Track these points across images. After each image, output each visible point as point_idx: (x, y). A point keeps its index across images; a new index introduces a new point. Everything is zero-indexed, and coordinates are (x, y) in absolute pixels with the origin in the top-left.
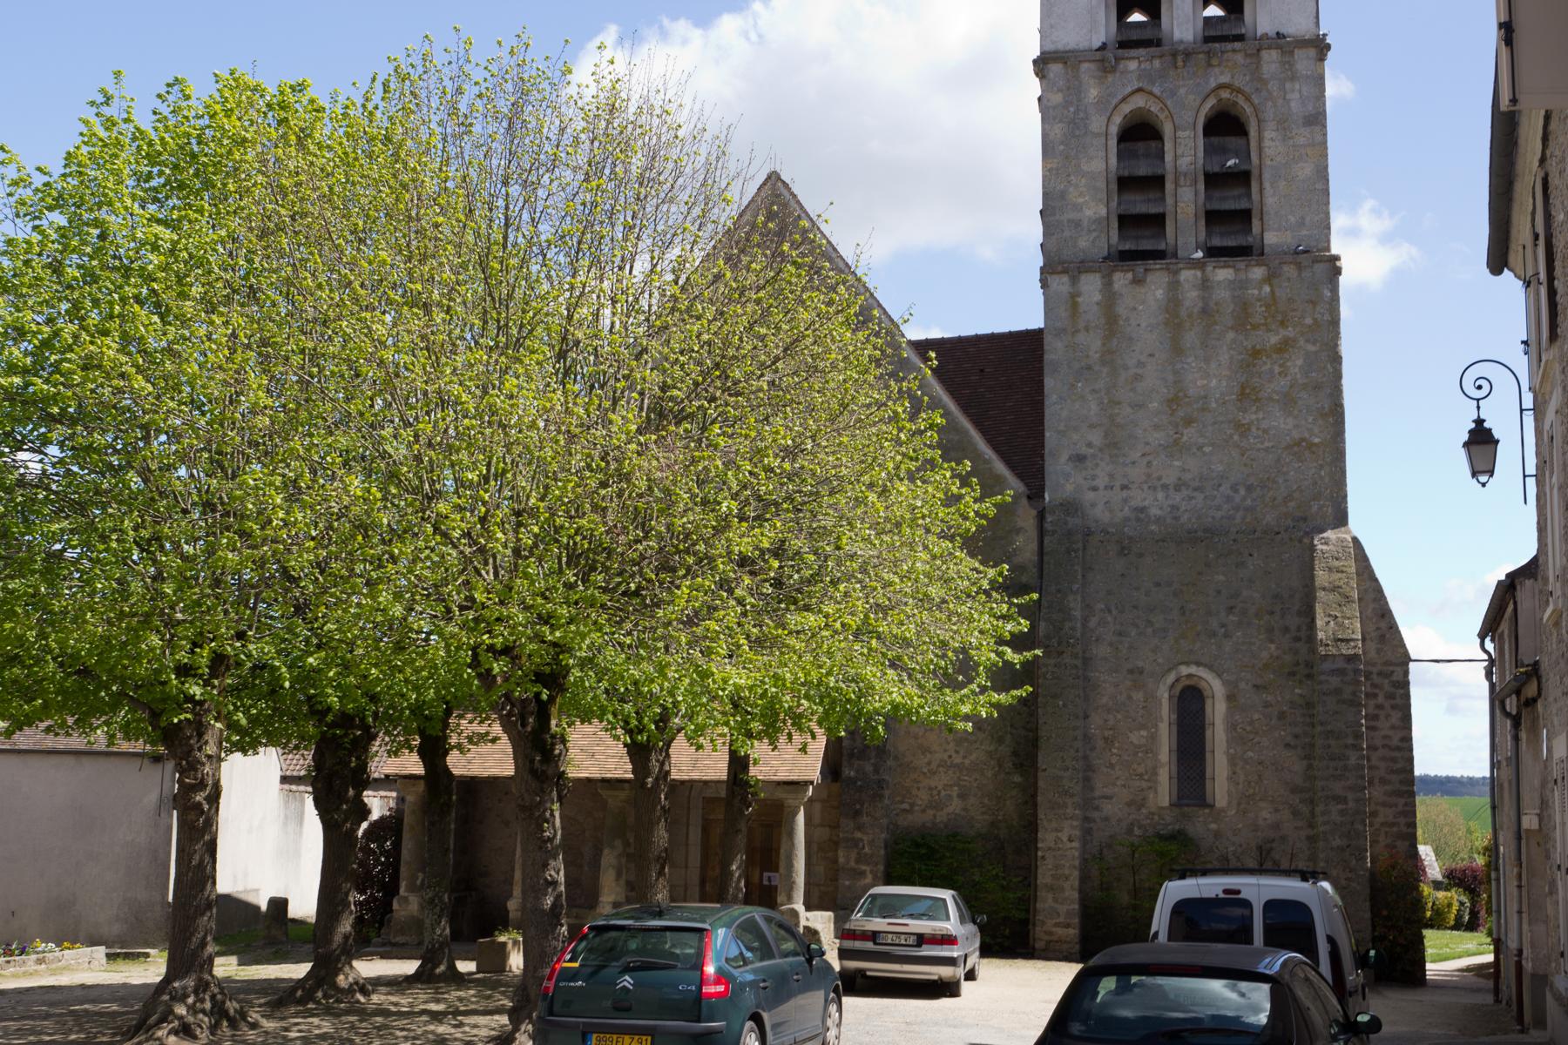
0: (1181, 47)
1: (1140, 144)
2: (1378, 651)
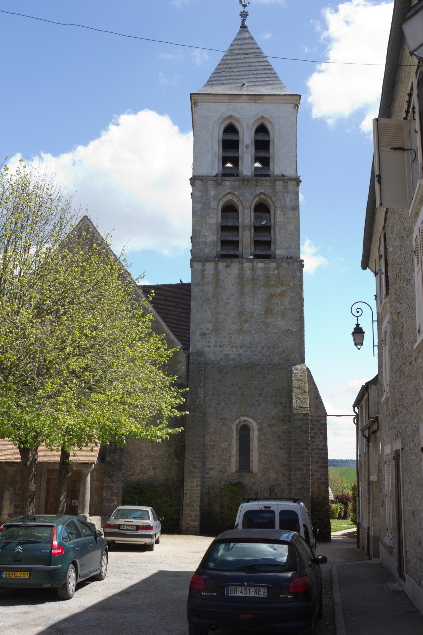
0: (246, 178)
1: (230, 213)
2: (316, 412)
